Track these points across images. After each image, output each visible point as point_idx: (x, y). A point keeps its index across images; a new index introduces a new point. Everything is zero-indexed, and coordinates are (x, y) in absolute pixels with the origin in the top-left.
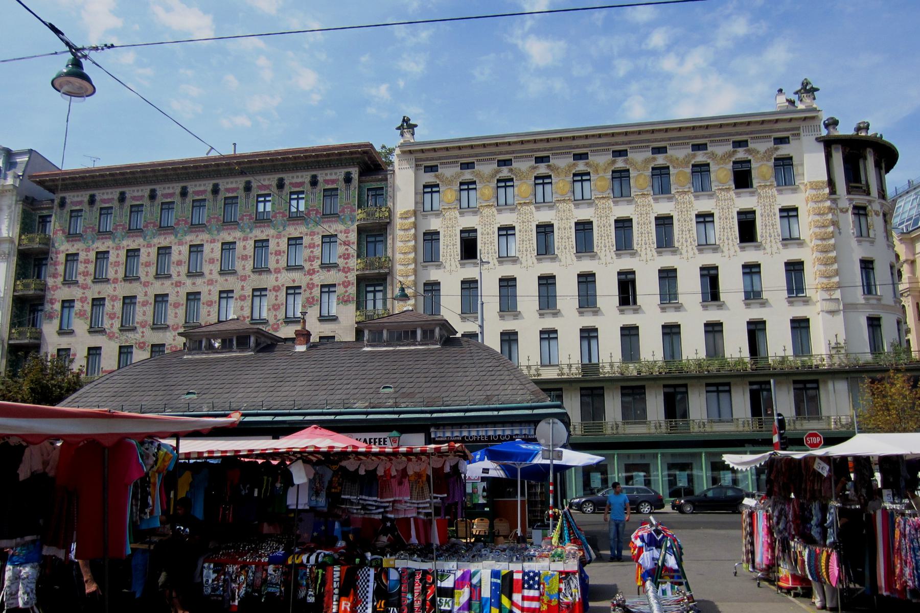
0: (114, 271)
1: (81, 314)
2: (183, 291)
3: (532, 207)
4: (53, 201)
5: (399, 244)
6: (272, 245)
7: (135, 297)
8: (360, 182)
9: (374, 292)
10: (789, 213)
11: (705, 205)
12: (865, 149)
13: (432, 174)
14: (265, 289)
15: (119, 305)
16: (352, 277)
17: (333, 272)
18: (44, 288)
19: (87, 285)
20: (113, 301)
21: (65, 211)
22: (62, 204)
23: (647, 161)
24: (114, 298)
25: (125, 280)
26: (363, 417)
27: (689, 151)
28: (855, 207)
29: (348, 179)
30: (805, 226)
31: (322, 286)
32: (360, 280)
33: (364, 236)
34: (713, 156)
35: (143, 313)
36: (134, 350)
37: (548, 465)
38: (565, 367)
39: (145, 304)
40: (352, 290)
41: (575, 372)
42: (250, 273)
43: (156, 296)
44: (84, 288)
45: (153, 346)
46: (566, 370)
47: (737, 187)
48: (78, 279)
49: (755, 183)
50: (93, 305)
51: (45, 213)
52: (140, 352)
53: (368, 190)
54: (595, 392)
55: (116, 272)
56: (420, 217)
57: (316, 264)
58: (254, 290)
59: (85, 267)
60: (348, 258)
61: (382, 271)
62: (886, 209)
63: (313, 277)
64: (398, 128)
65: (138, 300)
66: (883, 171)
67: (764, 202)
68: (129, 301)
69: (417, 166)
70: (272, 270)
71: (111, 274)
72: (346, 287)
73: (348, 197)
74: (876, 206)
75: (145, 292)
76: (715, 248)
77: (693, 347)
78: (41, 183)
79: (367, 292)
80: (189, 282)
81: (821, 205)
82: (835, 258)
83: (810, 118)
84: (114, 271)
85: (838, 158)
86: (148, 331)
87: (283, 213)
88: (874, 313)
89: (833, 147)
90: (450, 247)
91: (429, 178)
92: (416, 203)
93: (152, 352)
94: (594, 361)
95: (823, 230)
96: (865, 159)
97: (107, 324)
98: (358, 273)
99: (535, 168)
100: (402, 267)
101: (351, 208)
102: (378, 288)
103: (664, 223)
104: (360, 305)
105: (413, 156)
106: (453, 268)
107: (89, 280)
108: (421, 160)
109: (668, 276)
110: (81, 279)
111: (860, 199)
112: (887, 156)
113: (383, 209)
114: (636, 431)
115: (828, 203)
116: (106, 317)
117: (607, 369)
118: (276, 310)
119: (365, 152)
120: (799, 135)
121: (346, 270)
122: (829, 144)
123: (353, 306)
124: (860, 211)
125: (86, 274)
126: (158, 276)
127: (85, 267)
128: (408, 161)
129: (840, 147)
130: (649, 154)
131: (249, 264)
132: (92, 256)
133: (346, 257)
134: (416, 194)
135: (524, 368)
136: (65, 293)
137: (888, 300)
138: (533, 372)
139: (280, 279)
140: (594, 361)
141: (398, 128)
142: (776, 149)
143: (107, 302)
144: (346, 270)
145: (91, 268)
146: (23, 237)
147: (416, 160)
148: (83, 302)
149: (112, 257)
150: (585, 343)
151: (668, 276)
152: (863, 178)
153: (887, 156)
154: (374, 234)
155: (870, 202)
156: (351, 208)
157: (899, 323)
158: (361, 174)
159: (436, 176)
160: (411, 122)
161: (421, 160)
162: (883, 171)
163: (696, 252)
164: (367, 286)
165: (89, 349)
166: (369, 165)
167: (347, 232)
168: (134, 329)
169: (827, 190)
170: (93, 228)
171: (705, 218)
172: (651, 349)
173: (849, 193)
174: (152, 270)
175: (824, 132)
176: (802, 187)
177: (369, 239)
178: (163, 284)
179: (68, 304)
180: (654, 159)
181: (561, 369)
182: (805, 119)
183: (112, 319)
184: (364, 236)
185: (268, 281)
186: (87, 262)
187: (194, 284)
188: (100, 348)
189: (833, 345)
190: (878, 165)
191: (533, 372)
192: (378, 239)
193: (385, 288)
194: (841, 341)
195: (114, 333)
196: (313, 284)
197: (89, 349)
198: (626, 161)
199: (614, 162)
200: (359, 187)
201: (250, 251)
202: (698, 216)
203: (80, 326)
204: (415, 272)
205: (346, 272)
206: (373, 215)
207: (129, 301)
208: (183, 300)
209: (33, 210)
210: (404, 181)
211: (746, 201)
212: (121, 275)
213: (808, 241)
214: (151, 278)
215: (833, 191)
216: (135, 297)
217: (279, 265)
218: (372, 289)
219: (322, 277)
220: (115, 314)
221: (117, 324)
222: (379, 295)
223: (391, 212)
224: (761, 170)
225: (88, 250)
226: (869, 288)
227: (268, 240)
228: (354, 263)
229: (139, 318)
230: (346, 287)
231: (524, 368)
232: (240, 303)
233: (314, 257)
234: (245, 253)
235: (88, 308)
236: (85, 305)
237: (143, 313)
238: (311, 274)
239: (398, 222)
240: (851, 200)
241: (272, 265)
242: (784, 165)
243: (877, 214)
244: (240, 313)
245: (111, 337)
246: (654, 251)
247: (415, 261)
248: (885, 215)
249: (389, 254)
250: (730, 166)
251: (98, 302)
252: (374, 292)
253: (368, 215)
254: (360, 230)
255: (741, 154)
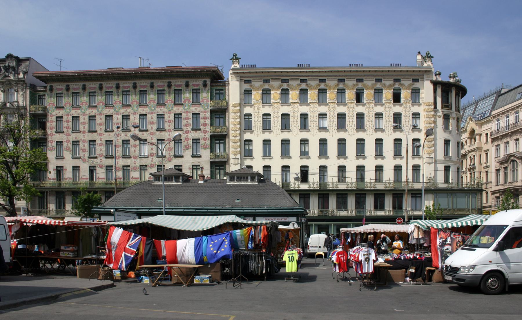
0: (83, 126)
1: (68, 149)
2: (120, 139)
3: (298, 105)
4: (45, 87)
5: (231, 120)
6: (166, 116)
7: (95, 141)
8: (211, 86)
9: (219, 143)
10: (416, 115)
11: (379, 109)
12: (452, 87)
13: (248, 84)
14: (164, 140)
15: (87, 145)
16: (208, 135)
17: (198, 132)
18: (45, 134)
19: (69, 133)
20: (84, 142)
21: (53, 93)
22: (51, 90)
23: (354, 85)
24: (84, 141)
25: (123, 158)
26: (230, 211)
27: (374, 82)
28: (445, 115)
29: (205, 85)
30: (423, 123)
31: (193, 139)
32: (212, 137)
33: (213, 114)
34: (384, 85)
35: (100, 149)
36: (97, 168)
37: (162, 185)
38: (312, 184)
39: (101, 145)
40: (208, 142)
41: (391, 186)
42: (155, 131)
43: (106, 141)
44: (68, 136)
45: (106, 166)
46: (312, 186)
47: (394, 102)
48: (64, 130)
49: (402, 100)
50: (73, 144)
51: (41, 94)
52: (100, 169)
53: (216, 90)
54: (344, 196)
55: (84, 128)
56: (242, 106)
57: (190, 128)
58: (158, 140)
59: (67, 124)
60: (206, 126)
61: (223, 134)
62: (459, 116)
63: (188, 134)
64: (231, 59)
65: (97, 143)
66: (460, 97)
67: (405, 109)
68: (92, 143)
69: (241, 79)
70: (167, 130)
71: (81, 128)
72: (205, 140)
73: (205, 97)
74: (454, 115)
75: (101, 138)
76: (382, 130)
77: (332, 179)
78: (38, 78)
79: (216, 143)
80: (123, 134)
81: (429, 113)
82: (434, 139)
83: (428, 72)
84: (83, 126)
85: (439, 91)
86: (103, 159)
87: (171, 100)
88: (448, 164)
89: (438, 86)
90: (257, 122)
91: (247, 86)
92: (240, 99)
93: (106, 169)
94: (288, 182)
95: (429, 125)
96: (451, 92)
97: (81, 154)
98: (212, 134)
99: (300, 85)
100: (233, 132)
101: (207, 100)
102: (221, 142)
103: (360, 116)
104: (213, 150)
105: (239, 75)
106: (259, 133)
107: (70, 131)
108: (243, 77)
109: (360, 143)
110: (65, 130)
111: (447, 111)
112: (462, 91)
113: (224, 102)
114: (343, 213)
115: (433, 113)
116: (81, 151)
117: (331, 186)
118: (169, 151)
119: (214, 71)
120: (423, 78)
121: (205, 132)
122: (435, 84)
123: (209, 151)
124: (446, 118)
125: (68, 128)
126: (106, 131)
127: (67, 124)
128: (236, 76)
129: (440, 86)
130: (355, 82)
131: (155, 127)
132: (70, 118)
133: (205, 125)
134: (240, 94)
135: (292, 184)
136: (58, 137)
137: (455, 158)
138: (372, 185)
139: (171, 135)
140: (288, 182)
141: (231, 59)
142: (413, 84)
143: (80, 143)
144: (205, 132)
145: (70, 125)
146: (32, 107)
147: (240, 77)
148: (68, 143)
149: (81, 119)
150: (378, 173)
151: (360, 143)
152: (450, 101)
153: (462, 91)
154: (219, 113)
155: (451, 113)
156: (207, 100)
157: (458, 169)
158: (211, 82)
159: (251, 86)
160: (237, 57)
161: (243, 77)
162: (460, 97)
163: (374, 131)
164: (216, 140)
165: (73, 167)
166: (215, 79)
167: (205, 112)
168: (96, 158)
169: (433, 107)
170: (70, 104)
171: (379, 116)
172: (388, 176)
173: (442, 108)
174: (103, 127)
175: (434, 79)
176: (422, 104)
177: (216, 116)
178: (109, 135)
179: (59, 143)
180: (357, 85)
181: (310, 185)
182: (426, 71)
183: (84, 152)
184: (213, 114)
185: (165, 135)
186: (68, 121)
187: (126, 135)
188: (79, 167)
189: (428, 178)
190: (457, 94)
191: (372, 185)
192: (221, 116)
193: (225, 142)
194: (432, 177)
195: (86, 160)
196: (188, 138)
197: (73, 167)
198: (344, 85)
199: (338, 85)
200: (211, 89)
201: (155, 119)
202: (376, 114)
203: (68, 155)
204: (240, 135)
205: (205, 133)
206: (219, 103)
207: (92, 143)
208: (121, 143)
209: (35, 91)
210: (234, 90)
211: (397, 109)
212: (87, 129)
213: (423, 130)
214: (103, 131)
215: (435, 107)
216: (95, 141)
217: (170, 128)
218: (218, 142)
219: (193, 135)
220: (85, 149)
221: (87, 155)
222: (222, 145)
223: (227, 103)
224: (405, 94)
225: (68, 115)
226: (446, 153)
227: (164, 114)
228: (208, 128)
229: (98, 152)
230: (205, 140)
231: (292, 184)
232: (151, 146)
233: (188, 124)
234: (153, 120)
235: (71, 145)
236: (69, 144)
237: (100, 149)
238: (187, 133)
239: (231, 109)
240: (442, 112)
241: (167, 127)
242: (416, 92)
243: (454, 119)
244: (151, 152)
245: (84, 161)
246: (355, 130)
247: (240, 129)
248: (458, 119)
249: (227, 125)
250: (391, 91)
251: (76, 143)
252: (219, 143)
253: (216, 103)
254: (212, 111)
255: (397, 86)
